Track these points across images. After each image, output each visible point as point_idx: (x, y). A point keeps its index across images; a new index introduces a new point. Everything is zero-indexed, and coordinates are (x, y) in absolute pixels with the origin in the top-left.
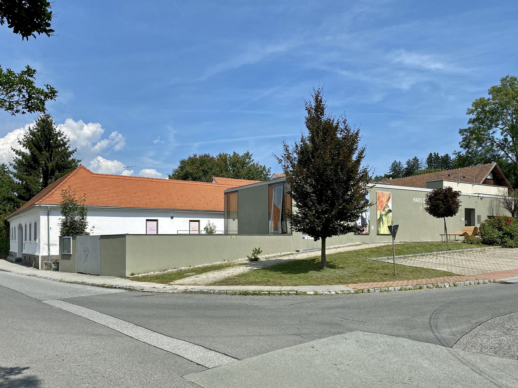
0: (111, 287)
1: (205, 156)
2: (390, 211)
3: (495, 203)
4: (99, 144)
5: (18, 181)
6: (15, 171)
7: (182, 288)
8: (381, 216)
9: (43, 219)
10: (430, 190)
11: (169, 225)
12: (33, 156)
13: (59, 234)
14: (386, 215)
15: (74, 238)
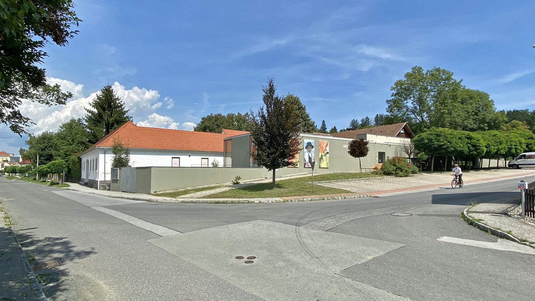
0: (139, 200)
1: (219, 115)
2: (328, 153)
3: (399, 148)
4: (156, 105)
5: (88, 130)
6: (86, 124)
7: (181, 200)
8: (322, 156)
9: (101, 156)
10: (351, 140)
11: (187, 161)
12: (99, 114)
13: (111, 167)
14: (325, 155)
15: (120, 169)
